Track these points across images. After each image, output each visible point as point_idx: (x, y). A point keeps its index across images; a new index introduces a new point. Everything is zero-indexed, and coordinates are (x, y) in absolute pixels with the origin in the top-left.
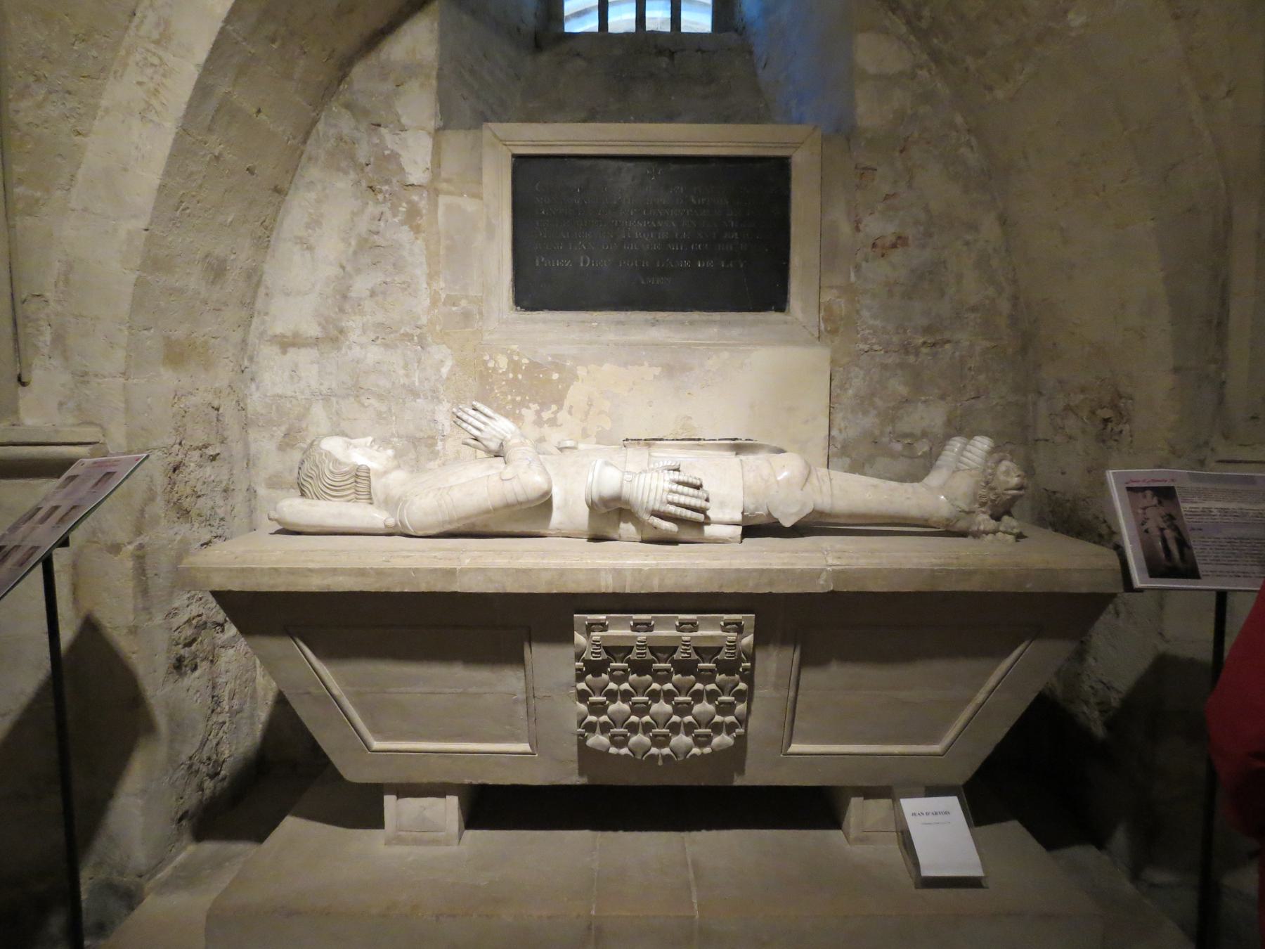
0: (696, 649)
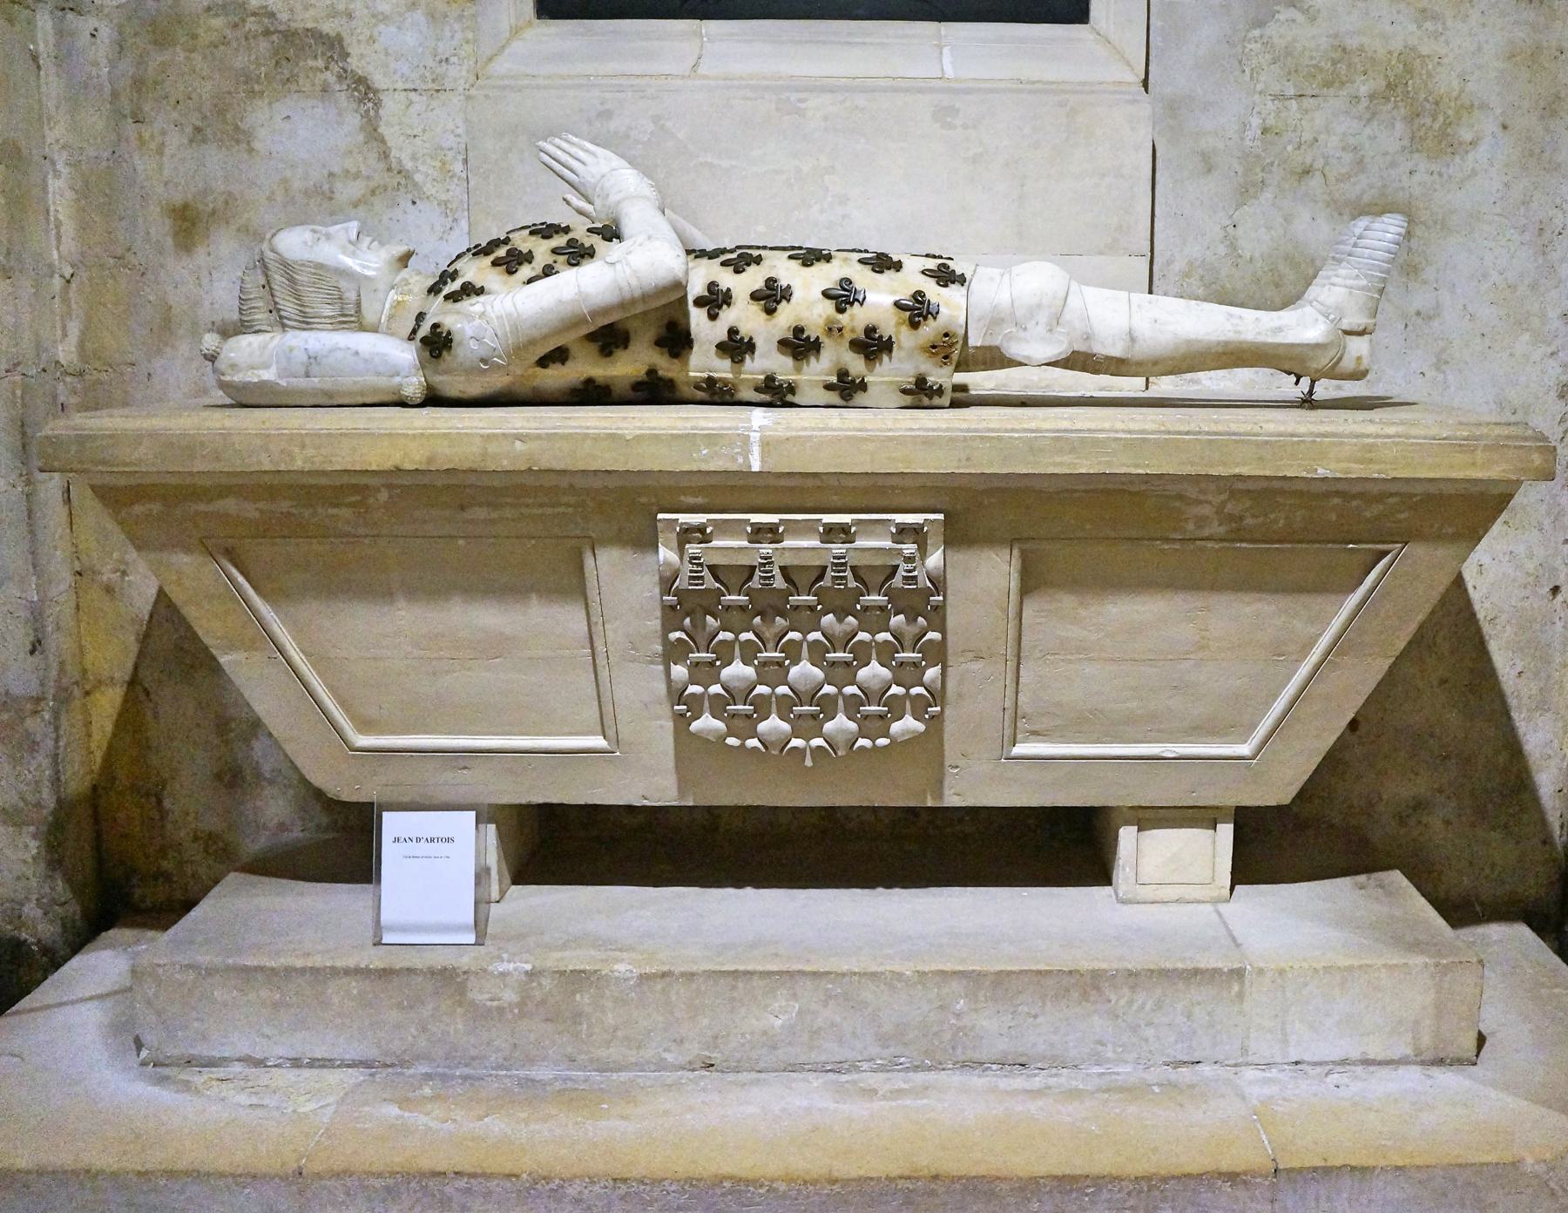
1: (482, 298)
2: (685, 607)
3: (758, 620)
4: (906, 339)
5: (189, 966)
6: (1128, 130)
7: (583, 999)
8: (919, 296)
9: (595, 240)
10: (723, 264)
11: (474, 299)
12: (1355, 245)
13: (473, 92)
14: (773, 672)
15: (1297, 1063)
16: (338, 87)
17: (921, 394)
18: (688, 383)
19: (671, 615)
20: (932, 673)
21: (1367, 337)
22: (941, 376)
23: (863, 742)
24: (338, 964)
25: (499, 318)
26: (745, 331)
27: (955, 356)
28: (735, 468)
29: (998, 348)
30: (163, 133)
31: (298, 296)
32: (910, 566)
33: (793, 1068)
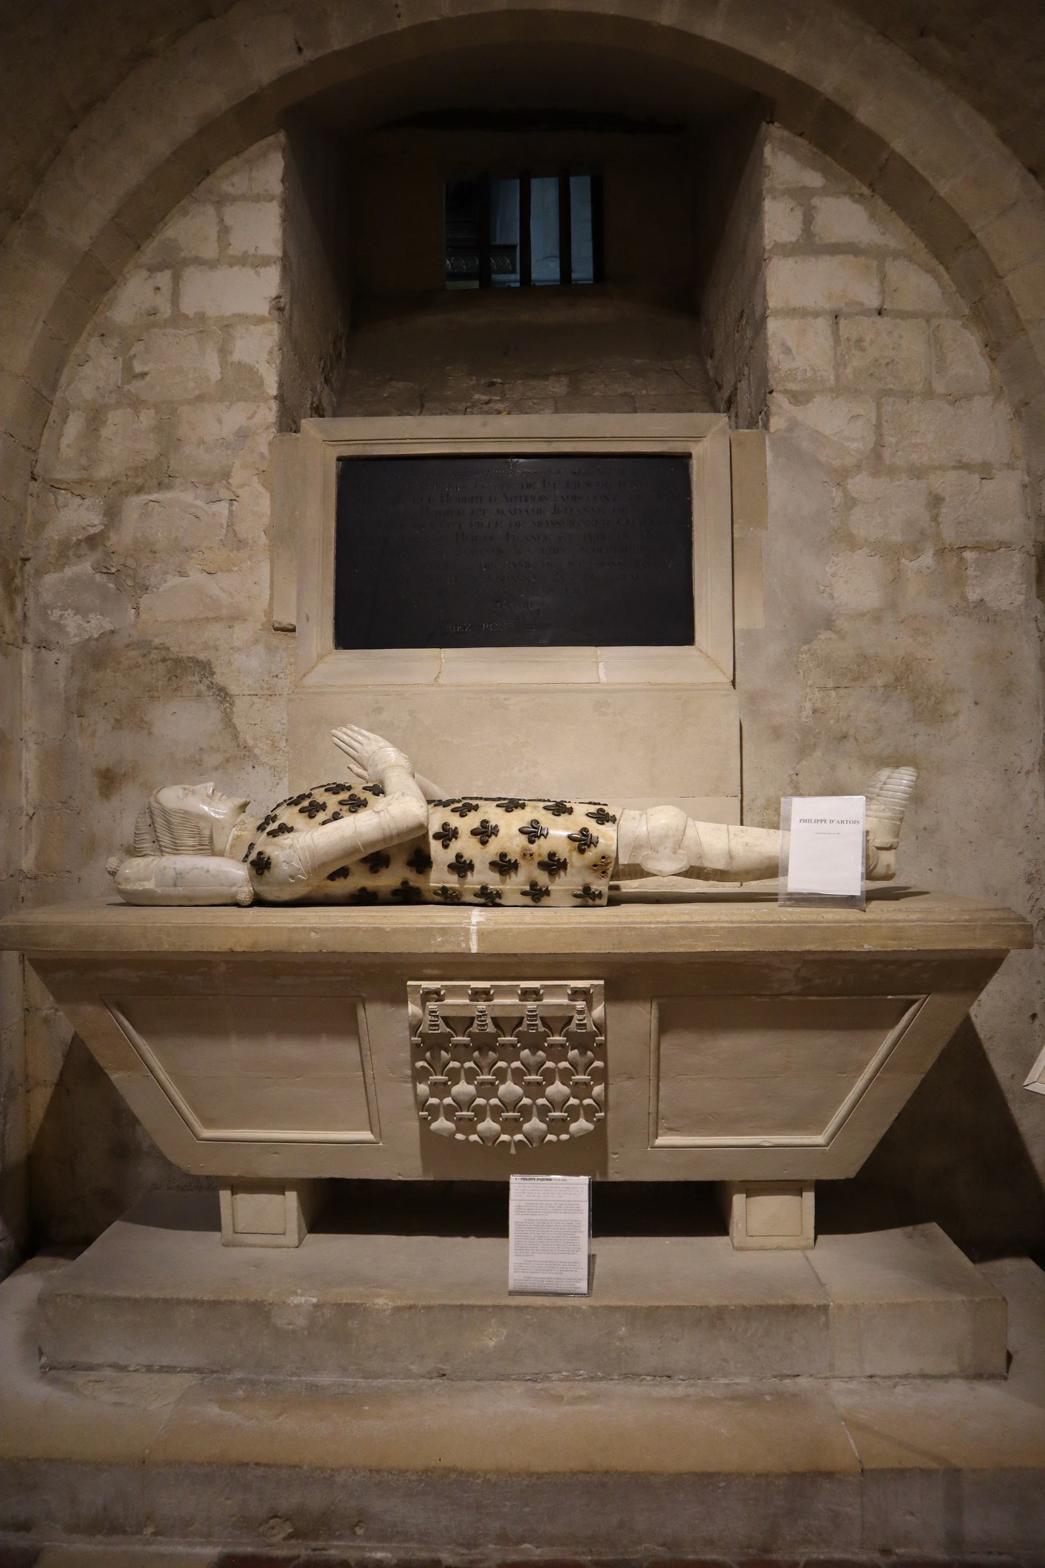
0: (446, 1019)
1: (291, 835)
2: (428, 1045)
3: (476, 1054)
4: (576, 860)
5: (78, 1296)
6: (724, 715)
7: (353, 1324)
8: (584, 831)
9: (368, 795)
10: (453, 811)
11: (286, 835)
12: (881, 789)
13: (293, 696)
14: (488, 1089)
15: (871, 1377)
16: (207, 694)
17: (586, 897)
18: (429, 891)
19: (417, 1051)
20: (598, 1089)
21: (893, 851)
22: (601, 885)
23: (551, 1137)
24: (182, 1296)
25: (302, 848)
26: (467, 856)
27: (610, 871)
28: (459, 951)
29: (638, 865)
30: (96, 723)
31: (171, 831)
32: (581, 1017)
33: (503, 1377)
